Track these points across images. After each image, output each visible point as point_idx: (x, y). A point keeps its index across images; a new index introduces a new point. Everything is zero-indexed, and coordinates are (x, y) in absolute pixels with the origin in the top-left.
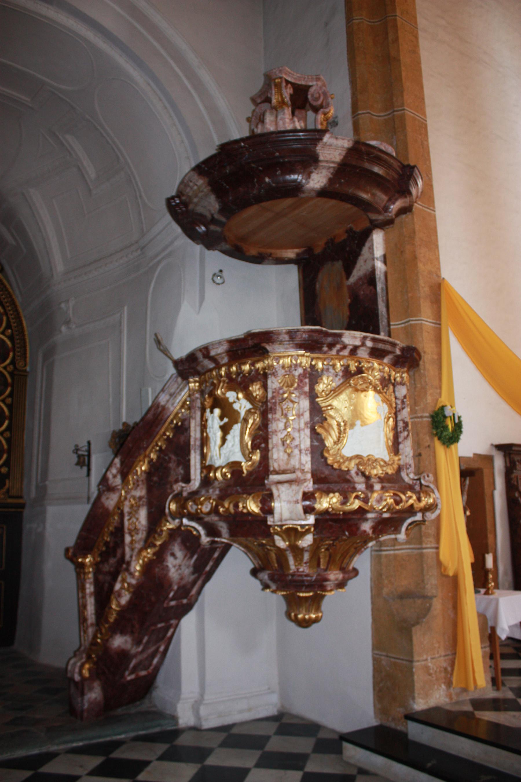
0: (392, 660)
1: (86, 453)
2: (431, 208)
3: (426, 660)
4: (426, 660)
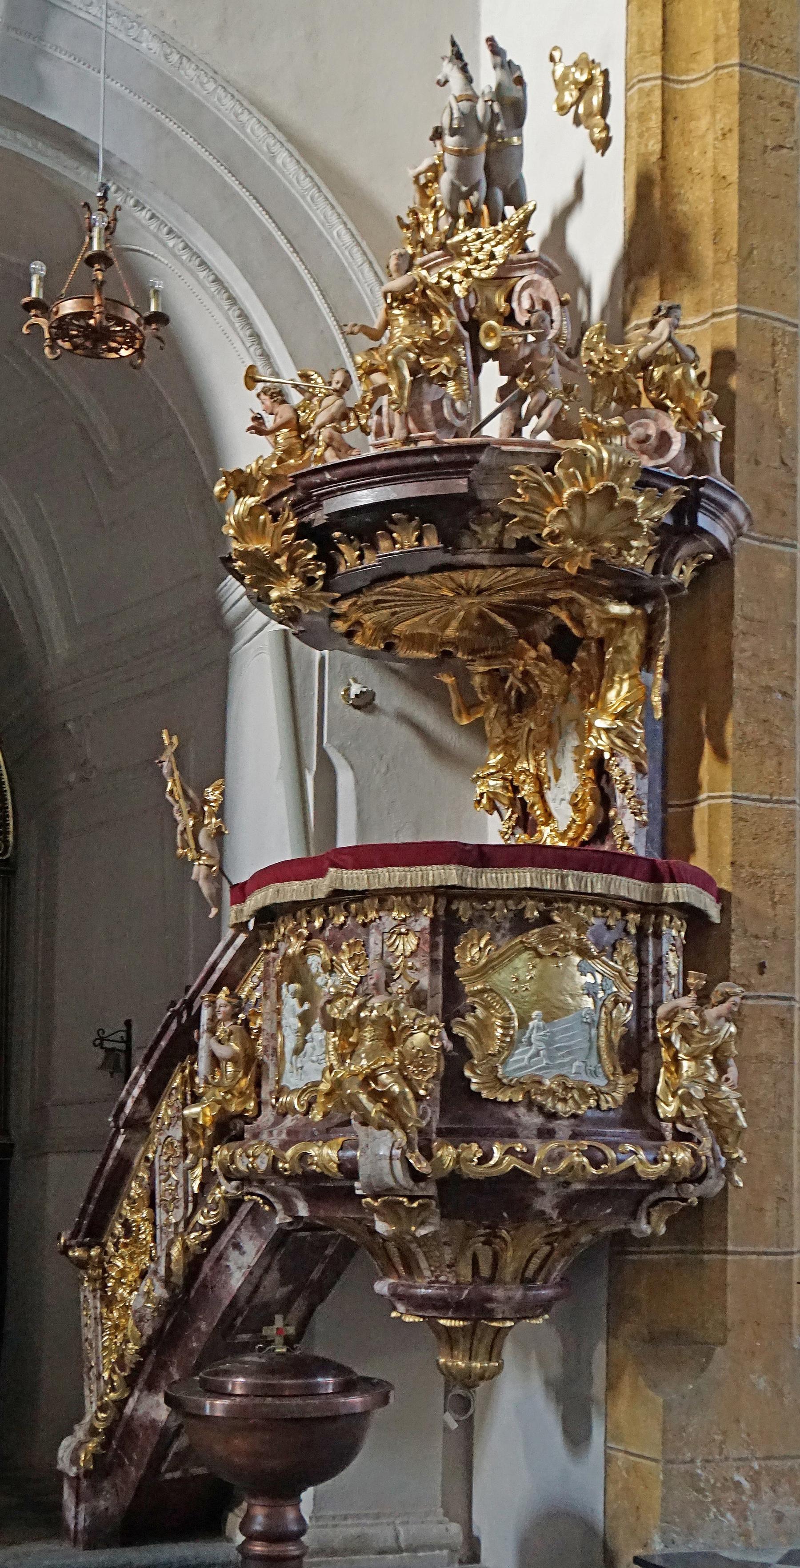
0: (632, 1458)
1: (122, 1046)
2: (786, 540)
3: (692, 1461)
4: (692, 1461)
